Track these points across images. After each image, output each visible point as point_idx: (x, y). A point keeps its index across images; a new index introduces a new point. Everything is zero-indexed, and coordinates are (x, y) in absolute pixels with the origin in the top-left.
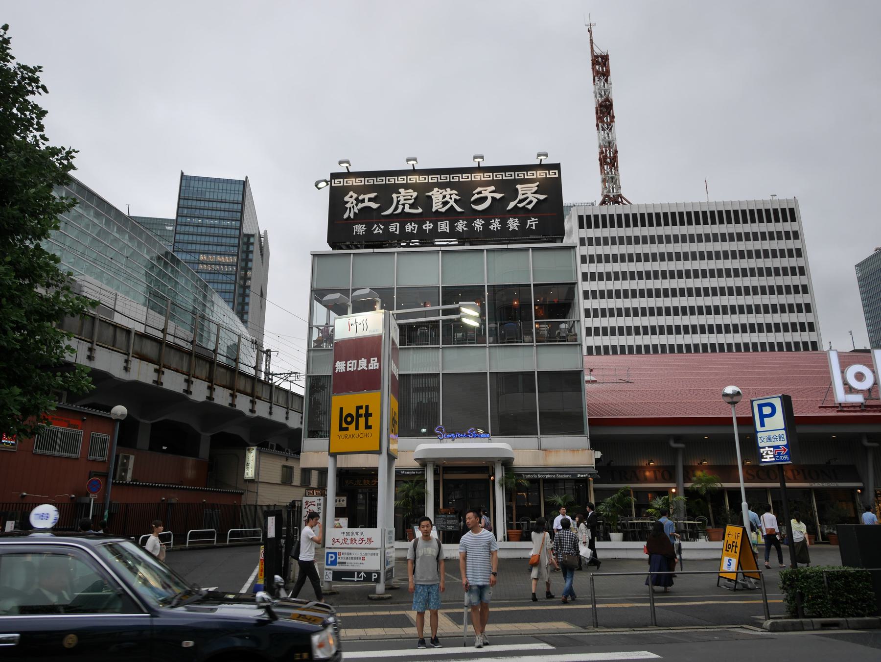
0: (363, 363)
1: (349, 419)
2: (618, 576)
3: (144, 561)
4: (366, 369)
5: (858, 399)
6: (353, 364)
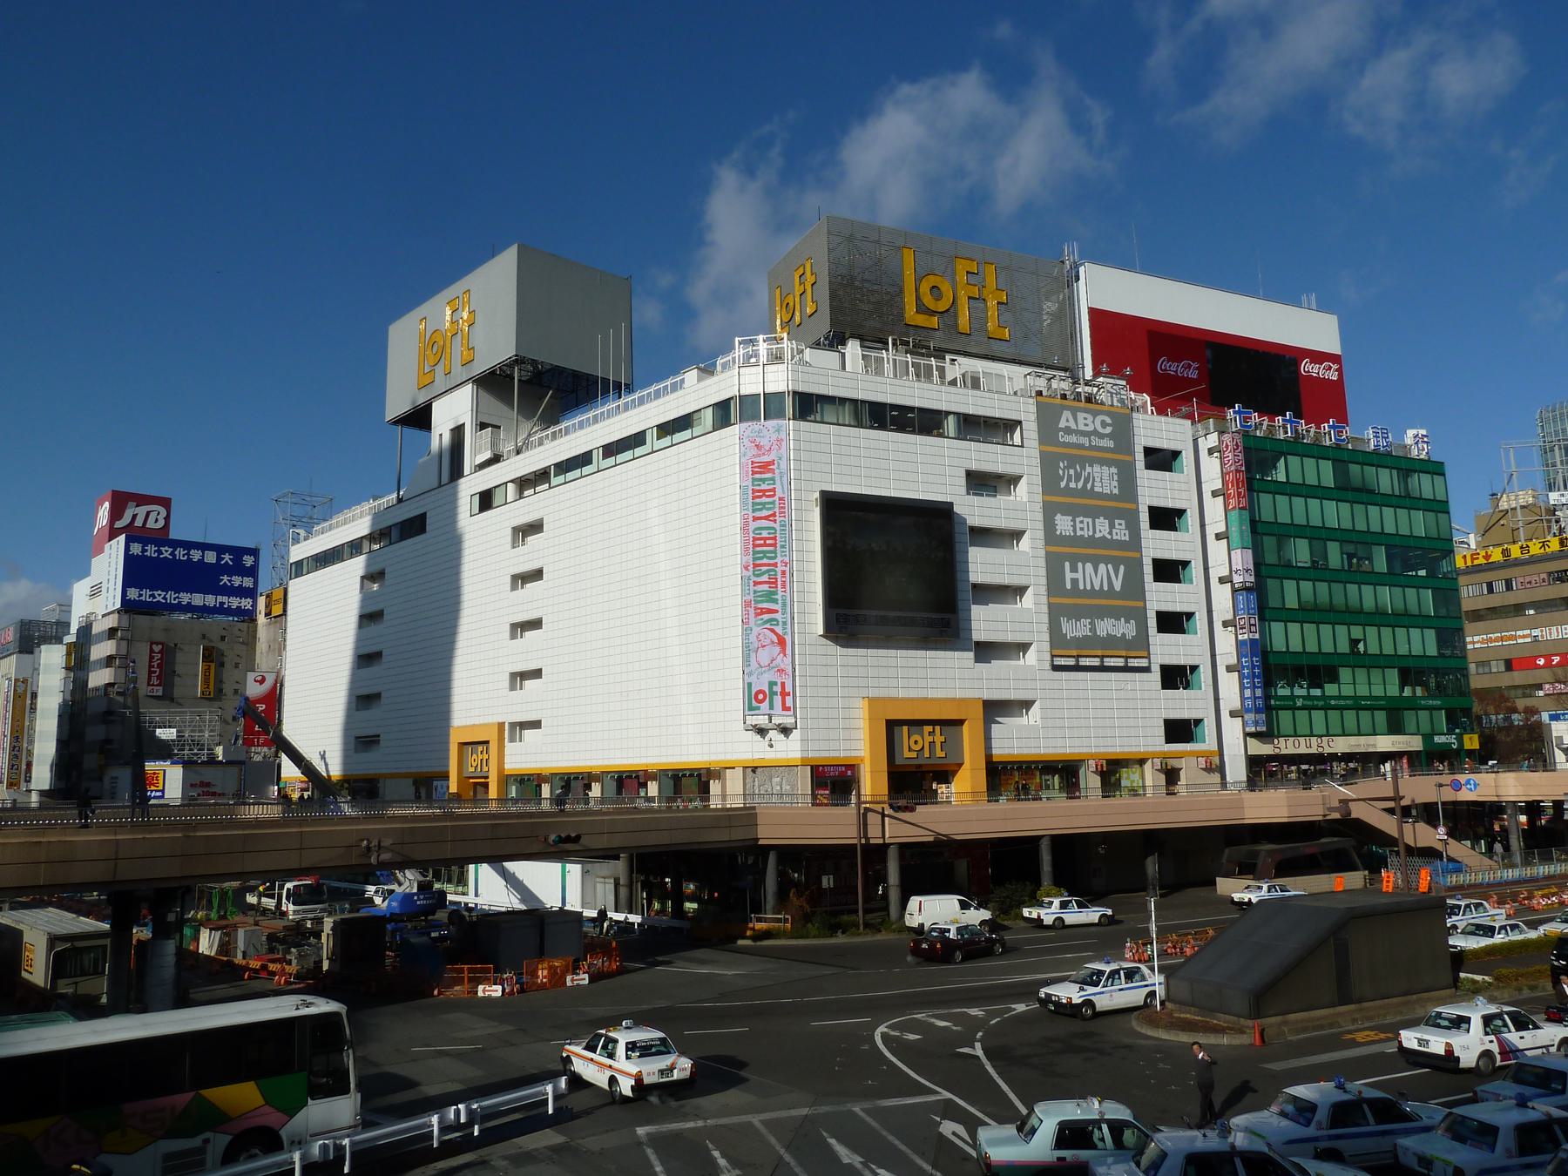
3: (557, 817)
4: (1109, 537)
5: (914, 755)
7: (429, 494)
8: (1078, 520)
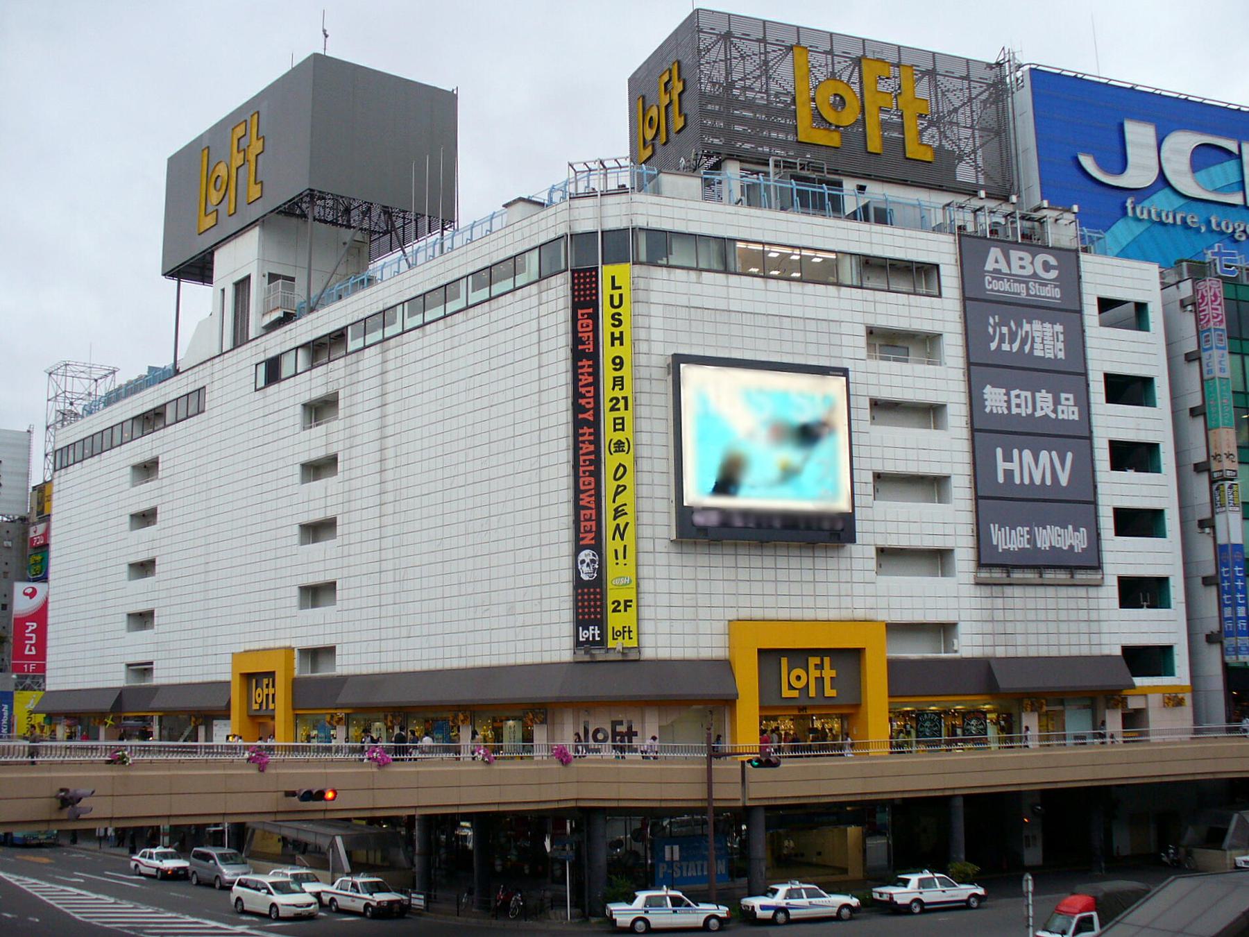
2: (259, 167)
4: (1053, 416)
5: (795, 694)
6: (1023, 398)
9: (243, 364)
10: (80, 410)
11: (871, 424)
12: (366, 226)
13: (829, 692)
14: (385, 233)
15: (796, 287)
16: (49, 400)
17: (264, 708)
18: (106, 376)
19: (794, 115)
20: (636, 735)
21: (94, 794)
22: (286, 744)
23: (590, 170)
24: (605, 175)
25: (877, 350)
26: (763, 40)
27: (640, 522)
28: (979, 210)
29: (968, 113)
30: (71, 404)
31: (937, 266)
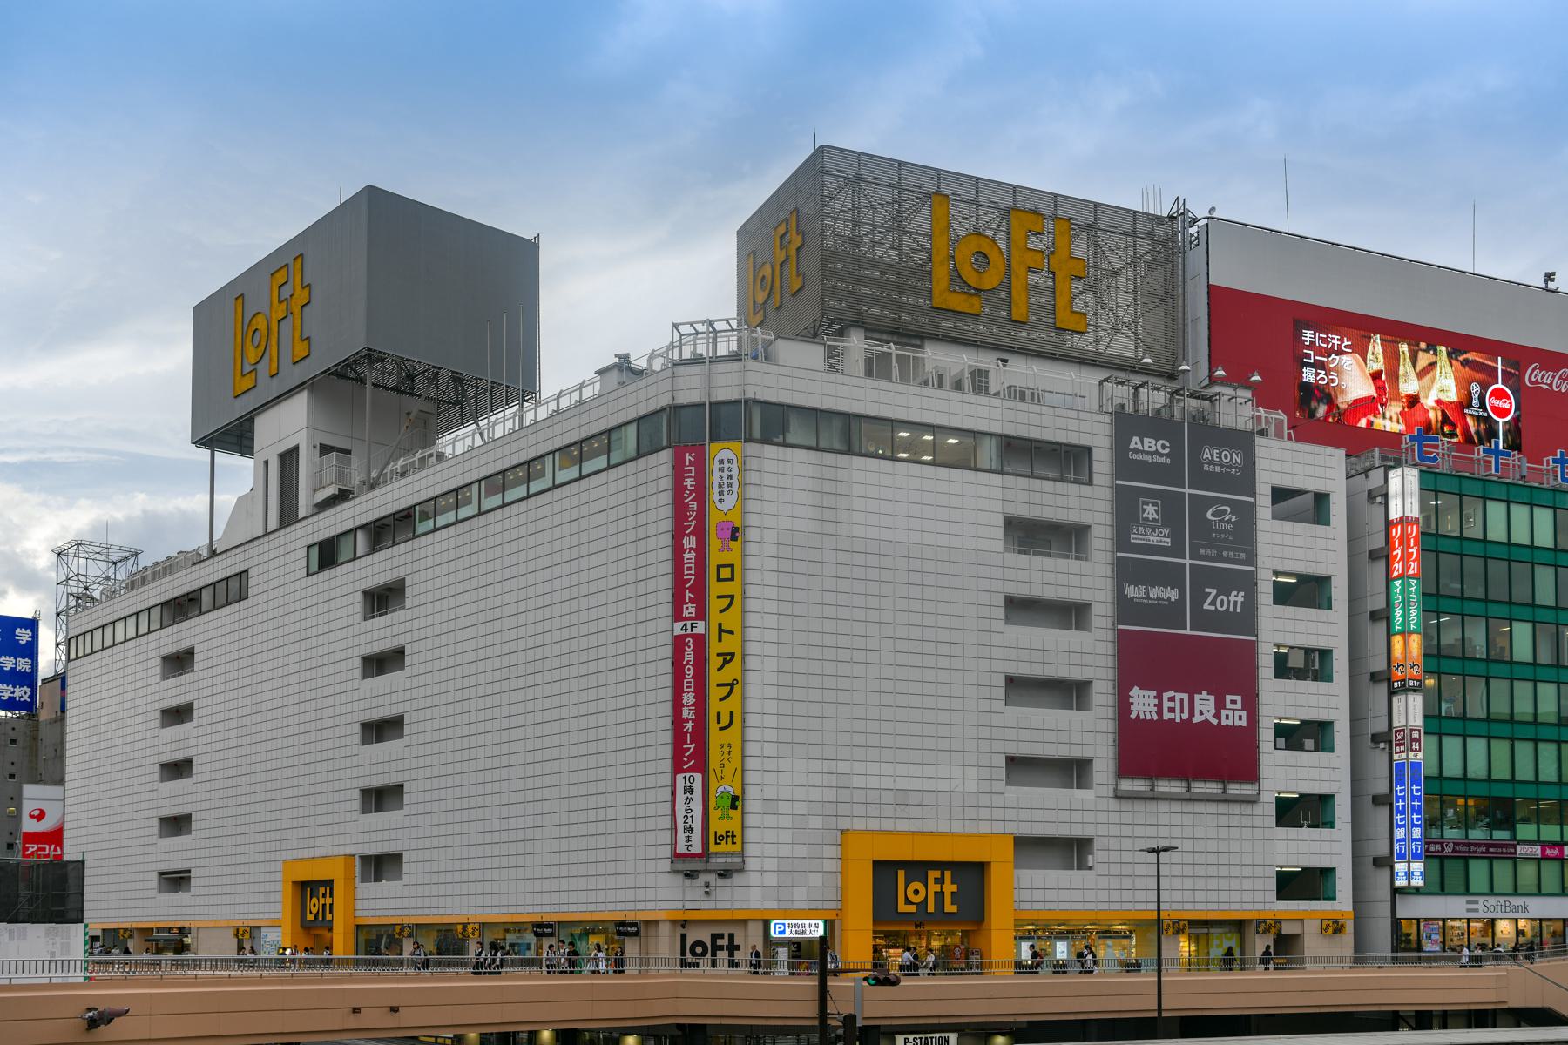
0: (1205, 706)
1: (699, 950)
4: (1215, 722)
5: (913, 909)
7: (251, 545)
8: (1166, 695)
9: (293, 546)
10: (97, 595)
11: (1006, 623)
12: (432, 394)
13: (950, 908)
14: (455, 404)
15: (930, 471)
16: (58, 584)
17: (321, 918)
18: (127, 558)
19: (929, 276)
20: (739, 950)
21: (129, 1013)
22: (346, 957)
23: (697, 333)
24: (715, 339)
25: (1016, 542)
26: (897, 186)
27: (746, 724)
28: (1141, 386)
29: (1131, 275)
30: (86, 588)
31: (1089, 449)
